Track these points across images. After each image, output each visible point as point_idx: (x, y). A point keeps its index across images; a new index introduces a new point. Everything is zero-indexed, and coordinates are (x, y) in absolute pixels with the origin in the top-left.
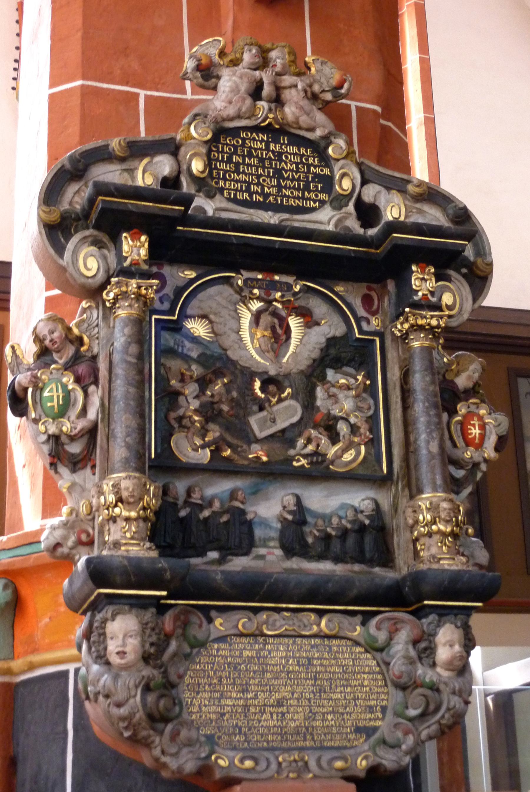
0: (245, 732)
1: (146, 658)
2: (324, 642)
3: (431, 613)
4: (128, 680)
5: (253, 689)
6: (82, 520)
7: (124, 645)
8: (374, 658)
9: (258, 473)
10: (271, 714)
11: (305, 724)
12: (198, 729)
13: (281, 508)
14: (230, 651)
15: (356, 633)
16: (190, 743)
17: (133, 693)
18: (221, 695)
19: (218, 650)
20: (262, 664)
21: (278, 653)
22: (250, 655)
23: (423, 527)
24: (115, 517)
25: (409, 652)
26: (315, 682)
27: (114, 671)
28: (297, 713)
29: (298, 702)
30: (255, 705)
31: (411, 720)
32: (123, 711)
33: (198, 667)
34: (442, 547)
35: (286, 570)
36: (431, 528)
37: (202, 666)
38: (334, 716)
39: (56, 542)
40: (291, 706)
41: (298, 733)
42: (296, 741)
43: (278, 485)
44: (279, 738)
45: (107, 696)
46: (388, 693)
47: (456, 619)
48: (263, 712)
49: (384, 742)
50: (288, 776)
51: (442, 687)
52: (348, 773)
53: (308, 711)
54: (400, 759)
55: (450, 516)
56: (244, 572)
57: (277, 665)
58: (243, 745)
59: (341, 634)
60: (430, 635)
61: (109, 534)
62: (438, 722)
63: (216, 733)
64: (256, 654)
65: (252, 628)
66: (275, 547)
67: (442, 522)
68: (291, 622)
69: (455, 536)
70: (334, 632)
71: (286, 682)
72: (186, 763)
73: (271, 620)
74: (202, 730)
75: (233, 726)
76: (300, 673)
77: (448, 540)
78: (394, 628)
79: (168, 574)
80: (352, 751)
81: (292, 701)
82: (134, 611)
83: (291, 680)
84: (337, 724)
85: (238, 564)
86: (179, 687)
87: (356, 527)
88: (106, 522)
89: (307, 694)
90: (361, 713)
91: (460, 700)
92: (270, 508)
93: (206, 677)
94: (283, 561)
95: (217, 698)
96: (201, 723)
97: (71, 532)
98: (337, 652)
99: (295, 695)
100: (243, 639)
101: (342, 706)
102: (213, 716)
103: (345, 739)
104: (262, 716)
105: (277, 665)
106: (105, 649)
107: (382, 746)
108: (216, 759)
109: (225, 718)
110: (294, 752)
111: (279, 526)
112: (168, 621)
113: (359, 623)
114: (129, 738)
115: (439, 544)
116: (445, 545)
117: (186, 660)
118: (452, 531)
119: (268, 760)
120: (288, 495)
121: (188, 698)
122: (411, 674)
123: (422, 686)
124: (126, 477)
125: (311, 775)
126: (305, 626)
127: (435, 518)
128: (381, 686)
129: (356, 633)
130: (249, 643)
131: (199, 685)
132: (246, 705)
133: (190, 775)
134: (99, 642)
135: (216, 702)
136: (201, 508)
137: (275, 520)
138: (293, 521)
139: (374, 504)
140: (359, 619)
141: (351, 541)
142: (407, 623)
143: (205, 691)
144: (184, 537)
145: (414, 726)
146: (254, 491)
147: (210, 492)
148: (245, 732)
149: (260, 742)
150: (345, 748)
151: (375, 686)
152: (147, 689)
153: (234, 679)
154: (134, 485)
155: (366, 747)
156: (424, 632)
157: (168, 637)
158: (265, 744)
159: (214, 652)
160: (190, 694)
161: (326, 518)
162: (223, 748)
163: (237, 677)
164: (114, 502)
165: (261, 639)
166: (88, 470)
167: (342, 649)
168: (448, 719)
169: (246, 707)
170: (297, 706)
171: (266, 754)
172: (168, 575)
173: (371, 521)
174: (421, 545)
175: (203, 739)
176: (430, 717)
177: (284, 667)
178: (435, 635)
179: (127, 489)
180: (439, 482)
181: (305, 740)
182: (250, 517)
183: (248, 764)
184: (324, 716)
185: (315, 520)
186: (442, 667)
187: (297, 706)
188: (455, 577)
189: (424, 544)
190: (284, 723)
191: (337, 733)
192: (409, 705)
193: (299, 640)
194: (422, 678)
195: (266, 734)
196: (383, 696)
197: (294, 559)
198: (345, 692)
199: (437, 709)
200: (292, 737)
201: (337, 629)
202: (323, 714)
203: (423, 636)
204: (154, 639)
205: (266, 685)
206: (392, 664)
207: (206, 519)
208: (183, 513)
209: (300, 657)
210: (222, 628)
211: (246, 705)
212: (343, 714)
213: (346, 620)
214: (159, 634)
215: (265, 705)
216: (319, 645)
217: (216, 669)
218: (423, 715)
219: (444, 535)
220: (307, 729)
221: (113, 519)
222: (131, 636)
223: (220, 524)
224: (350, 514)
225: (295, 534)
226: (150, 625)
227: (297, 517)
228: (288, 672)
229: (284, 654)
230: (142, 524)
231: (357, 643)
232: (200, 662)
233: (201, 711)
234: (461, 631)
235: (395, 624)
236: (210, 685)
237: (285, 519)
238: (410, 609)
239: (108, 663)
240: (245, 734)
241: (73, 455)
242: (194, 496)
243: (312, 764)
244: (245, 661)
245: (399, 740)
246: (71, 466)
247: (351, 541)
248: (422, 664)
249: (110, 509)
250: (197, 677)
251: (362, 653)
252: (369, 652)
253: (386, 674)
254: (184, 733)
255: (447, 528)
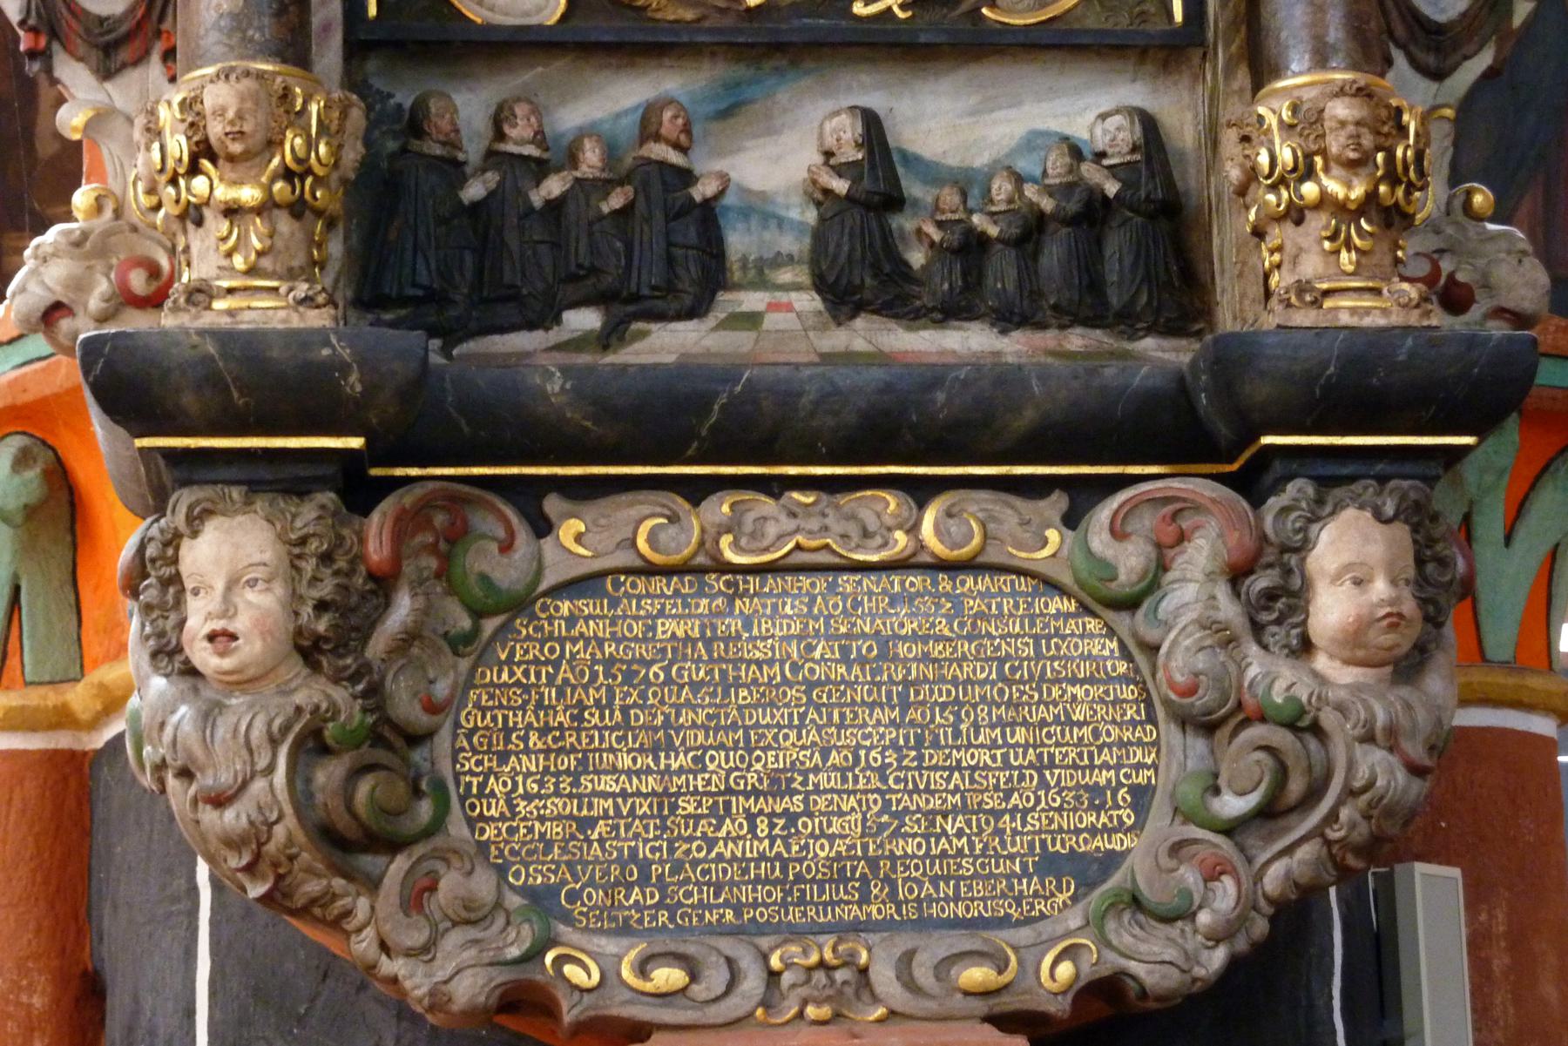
0: (660, 877)
1: (309, 650)
2: (935, 583)
3: (1290, 477)
4: (247, 717)
5: (690, 743)
6: (135, 229)
7: (228, 611)
8: (1111, 633)
9: (731, 45)
10: (751, 818)
11: (865, 847)
12: (501, 871)
13: (818, 159)
14: (613, 624)
15: (1046, 552)
16: (471, 916)
17: (262, 763)
18: (583, 762)
19: (571, 621)
20: (721, 659)
21: (779, 621)
22: (680, 634)
23: (1273, 188)
24: (198, 207)
25: (1217, 609)
26: (903, 714)
27: (208, 693)
28: (841, 814)
29: (844, 780)
30: (696, 792)
31: (1231, 829)
32: (233, 818)
33: (505, 676)
34: (1337, 252)
35: (828, 358)
36: (1297, 190)
37: (519, 673)
38: (968, 823)
39: (49, 299)
40: (817, 790)
41: (842, 879)
42: (833, 903)
43: (806, 82)
44: (778, 895)
45: (186, 774)
46: (1156, 743)
47: (1379, 493)
48: (720, 814)
49: (1136, 902)
50: (800, 1015)
51: (1328, 719)
52: (1008, 1003)
53: (876, 809)
54: (1192, 958)
55: (1358, 147)
56: (685, 369)
57: (770, 662)
58: (654, 918)
59: (992, 556)
60: (1285, 549)
61: (189, 265)
62: (1317, 832)
63: (564, 882)
64: (703, 627)
65: (683, 543)
66: (797, 287)
67: (1336, 170)
68: (814, 524)
69: (1393, 219)
70: (964, 552)
71: (802, 717)
72: (461, 975)
73: (749, 518)
74: (517, 875)
75: (619, 860)
76: (849, 684)
77: (1359, 229)
78: (1171, 529)
79: (354, 378)
80: (1024, 935)
81: (822, 777)
82: (261, 504)
83: (818, 708)
84: (979, 846)
85: (667, 343)
86: (436, 739)
87: (1073, 207)
88: (176, 226)
89: (873, 754)
90: (1060, 810)
91: (1394, 760)
92: (778, 160)
93: (531, 707)
94: (824, 328)
95: (568, 772)
96: (512, 852)
97: (99, 266)
98: (981, 615)
99: (835, 758)
100: (658, 584)
101: (997, 788)
102: (554, 830)
103: (1003, 895)
104: (718, 828)
105: (770, 662)
106: (181, 624)
107: (1126, 916)
108: (560, 961)
109: (595, 836)
110: (821, 938)
111: (811, 216)
112: (376, 534)
113: (1057, 519)
114: (266, 899)
115: (1327, 245)
116: (1348, 245)
117: (456, 653)
118: (1371, 196)
119: (730, 962)
120: (837, 113)
121: (471, 773)
122: (1229, 683)
123: (1263, 719)
124: (218, 75)
125: (880, 1011)
126: (866, 534)
127: (1309, 157)
128: (1134, 723)
129: (1046, 552)
130: (677, 593)
131: (507, 731)
132: (666, 793)
133: (471, 1014)
134: (163, 607)
135: (565, 786)
136: (540, 169)
137: (796, 199)
138: (849, 197)
139: (1138, 128)
140: (1057, 503)
141: (1054, 254)
142: (1207, 511)
143: (527, 751)
144: (479, 272)
145: (1242, 849)
146: (723, 105)
147: (571, 117)
148: (660, 877)
149: (710, 907)
150: (1004, 922)
151: (1114, 722)
152: (313, 743)
153: (625, 710)
154: (242, 99)
155: (1074, 920)
156: (1264, 538)
157: (383, 585)
158: (729, 915)
159: (560, 627)
160: (479, 763)
161: (966, 182)
162: (586, 929)
163: (635, 705)
164: (186, 158)
165: (717, 583)
166: (154, 69)
167: (999, 606)
168: (1353, 826)
169: (666, 800)
170: (839, 792)
171: (726, 945)
172: (354, 383)
173: (1126, 185)
174: (1272, 252)
175: (514, 901)
176: (1293, 818)
177: (795, 668)
178: (1303, 547)
179: (220, 112)
180: (1335, 33)
181: (865, 900)
182: (704, 190)
183: (667, 977)
184: (933, 824)
185: (935, 191)
186: (1331, 656)
187: (839, 792)
188: (1367, 349)
189: (1279, 249)
190: (795, 848)
191: (975, 876)
192: (1222, 782)
193: (847, 582)
194: (1260, 691)
195: (732, 883)
196: (1139, 755)
197: (860, 323)
198: (1006, 744)
199: (1313, 795)
200: (821, 892)
201: (976, 541)
202: (930, 815)
203: (1259, 553)
204: (326, 590)
205: (734, 727)
206: (1163, 650)
207: (555, 206)
208: (474, 191)
209: (848, 636)
210: (581, 551)
211: (666, 793)
212: (997, 814)
213: (1010, 513)
214: (350, 573)
215: (729, 791)
216: (919, 594)
217: (566, 681)
218: (1270, 813)
219: (1340, 208)
220: (873, 863)
221: (193, 215)
222: (252, 583)
223: (601, 218)
224: (1057, 165)
225: (866, 239)
226: (313, 545)
227: (866, 183)
228: (811, 685)
229: (796, 628)
230: (285, 224)
231: (1053, 586)
232: (510, 661)
233: (514, 814)
234: (1401, 531)
235: (1175, 515)
236: (544, 731)
237: (827, 192)
238: (1228, 468)
239: (191, 671)
240: (662, 885)
241: (101, 20)
242: (512, 133)
243: (884, 976)
244: (664, 650)
245: (1187, 894)
246: (95, 55)
247: (1054, 254)
248: (1265, 647)
249: (182, 182)
250: (501, 706)
251: (1068, 616)
252: (1094, 615)
253: (1150, 685)
254: (450, 883)
255: (1349, 186)
